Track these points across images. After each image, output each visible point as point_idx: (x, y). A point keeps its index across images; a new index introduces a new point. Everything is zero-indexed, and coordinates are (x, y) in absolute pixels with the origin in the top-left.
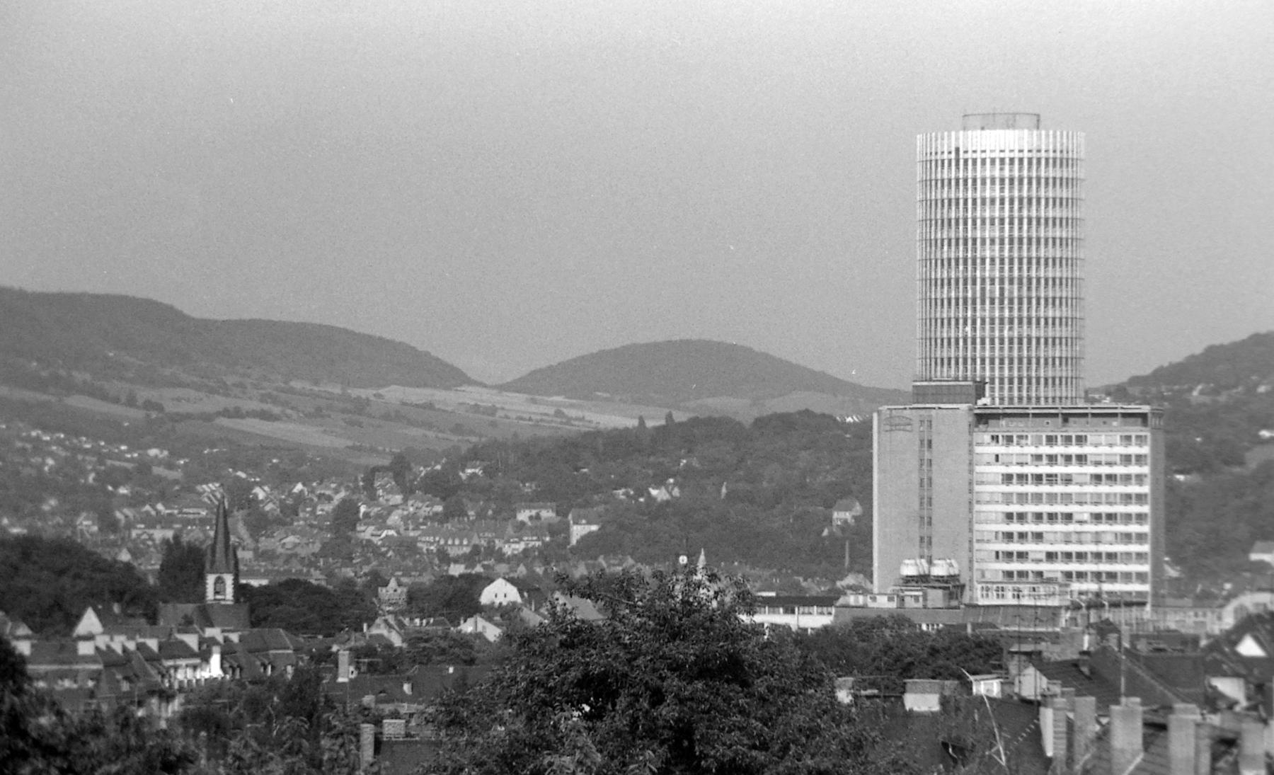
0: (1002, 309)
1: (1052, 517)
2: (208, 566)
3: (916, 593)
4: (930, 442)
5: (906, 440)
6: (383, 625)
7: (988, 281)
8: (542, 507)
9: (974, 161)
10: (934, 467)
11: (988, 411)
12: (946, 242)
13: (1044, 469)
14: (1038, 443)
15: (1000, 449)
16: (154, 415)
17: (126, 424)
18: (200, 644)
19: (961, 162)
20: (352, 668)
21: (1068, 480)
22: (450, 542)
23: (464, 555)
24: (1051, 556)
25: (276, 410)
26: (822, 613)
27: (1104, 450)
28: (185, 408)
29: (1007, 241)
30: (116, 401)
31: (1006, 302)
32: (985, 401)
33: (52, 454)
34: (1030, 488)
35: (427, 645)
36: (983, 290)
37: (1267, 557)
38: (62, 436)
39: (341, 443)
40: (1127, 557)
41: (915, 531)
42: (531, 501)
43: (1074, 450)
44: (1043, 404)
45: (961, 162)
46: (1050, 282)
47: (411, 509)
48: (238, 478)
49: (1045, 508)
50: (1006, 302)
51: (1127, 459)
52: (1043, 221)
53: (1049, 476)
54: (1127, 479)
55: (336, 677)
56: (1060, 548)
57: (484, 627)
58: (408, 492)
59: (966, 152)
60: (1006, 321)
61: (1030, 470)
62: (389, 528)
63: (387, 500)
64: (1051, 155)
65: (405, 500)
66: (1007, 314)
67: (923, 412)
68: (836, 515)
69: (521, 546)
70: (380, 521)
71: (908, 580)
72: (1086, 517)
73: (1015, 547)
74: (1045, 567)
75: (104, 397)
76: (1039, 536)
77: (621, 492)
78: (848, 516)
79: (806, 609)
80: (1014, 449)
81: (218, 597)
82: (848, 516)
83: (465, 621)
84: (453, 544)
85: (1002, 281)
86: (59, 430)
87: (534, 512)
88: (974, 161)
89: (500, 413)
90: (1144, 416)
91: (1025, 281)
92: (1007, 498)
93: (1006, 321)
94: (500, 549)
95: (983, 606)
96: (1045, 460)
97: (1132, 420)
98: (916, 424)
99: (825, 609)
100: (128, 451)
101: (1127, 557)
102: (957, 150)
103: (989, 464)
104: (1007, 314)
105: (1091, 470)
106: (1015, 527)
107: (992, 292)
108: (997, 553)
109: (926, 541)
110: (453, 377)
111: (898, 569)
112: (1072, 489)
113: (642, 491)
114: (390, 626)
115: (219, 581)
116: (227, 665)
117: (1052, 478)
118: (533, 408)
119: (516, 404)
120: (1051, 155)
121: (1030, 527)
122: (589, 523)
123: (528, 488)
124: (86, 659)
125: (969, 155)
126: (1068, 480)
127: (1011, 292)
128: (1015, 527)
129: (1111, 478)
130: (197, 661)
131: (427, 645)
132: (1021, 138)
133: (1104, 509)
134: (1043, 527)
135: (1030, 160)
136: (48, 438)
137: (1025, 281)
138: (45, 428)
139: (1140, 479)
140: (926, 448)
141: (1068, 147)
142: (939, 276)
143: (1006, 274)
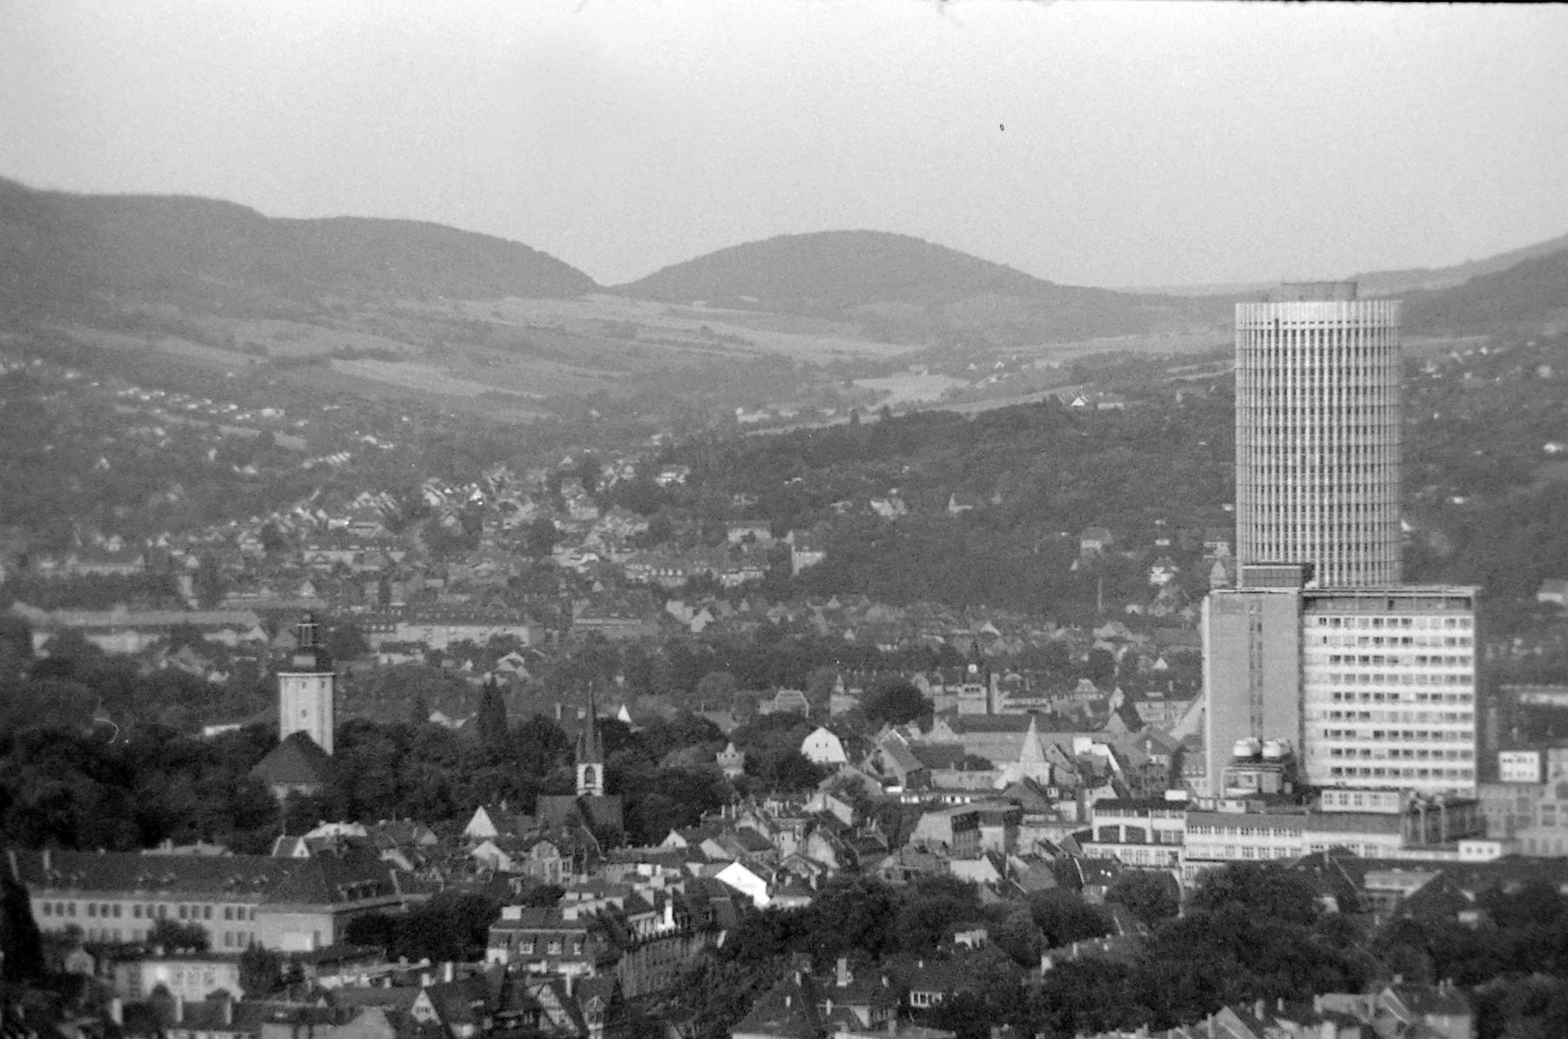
0: (1322, 477)
1: (1378, 696)
2: (578, 756)
3: (1250, 773)
4: (1260, 626)
5: (1238, 624)
6: (751, 818)
7: (1308, 451)
8: (756, 526)
9: (1294, 332)
10: (1264, 650)
11: (1317, 595)
12: (1266, 411)
13: (1371, 650)
14: (1364, 624)
15: (1327, 631)
16: (259, 360)
17: (230, 374)
18: (655, 897)
19: (1281, 333)
20: (849, 974)
21: (1394, 661)
22: (663, 573)
23: (679, 588)
24: (1378, 734)
25: (392, 346)
26: (1174, 817)
27: (1429, 633)
28: (292, 349)
29: (1326, 410)
30: (213, 343)
31: (1326, 470)
32: (1312, 585)
33: (161, 424)
34: (1358, 669)
35: (848, 891)
36: (1303, 458)
37: (1557, 598)
38: (163, 394)
39: (474, 389)
40: (1453, 736)
41: (1246, 711)
42: (747, 516)
43: (1400, 632)
44: (1370, 586)
45: (1281, 333)
46: (1369, 449)
47: (609, 526)
48: (367, 443)
49: (1372, 688)
50: (1326, 470)
51: (1451, 642)
52: (1361, 390)
53: (1405, 677)
54: (1451, 660)
55: (835, 982)
56: (1387, 727)
57: (833, 805)
58: (604, 503)
59: (1285, 323)
60: (1326, 489)
61: (1357, 651)
62: (589, 551)
63: (581, 514)
64: (1369, 325)
65: (602, 514)
66: (1326, 481)
67: (1253, 597)
68: (1085, 544)
69: (741, 577)
70: (577, 541)
71: (1241, 761)
72: (1412, 697)
73: (1343, 725)
74: (1372, 745)
75: (200, 338)
76: (1366, 715)
77: (839, 504)
78: (1097, 545)
79: (1160, 812)
80: (1342, 631)
81: (589, 785)
82: (1097, 545)
83: (811, 797)
84: (666, 575)
85: (1322, 449)
86: (159, 386)
87: (746, 532)
88: (1294, 332)
89: (640, 335)
90: (1467, 600)
91: (1344, 449)
92: (1335, 678)
93: (1326, 489)
94: (718, 580)
95: (1327, 813)
96: (1371, 642)
97: (1456, 603)
98: (1247, 606)
99: (1177, 813)
100: (241, 410)
101: (1453, 736)
102: (1277, 321)
103: (1317, 645)
104: (1326, 481)
105: (1415, 651)
106: (1344, 707)
107: (1312, 460)
108: (1326, 731)
109: (1257, 721)
110: (571, 282)
111: (1231, 752)
112: (1398, 670)
113: (862, 503)
114: (758, 820)
115: (589, 770)
116: (678, 916)
117: (1378, 659)
118: (677, 324)
119: (649, 312)
120: (1369, 325)
121: (1358, 707)
122: (812, 550)
123: (740, 500)
124: (570, 925)
125: (1289, 327)
126: (1394, 661)
127: (1331, 460)
128: (1344, 707)
129: (1436, 659)
130: (653, 914)
131: (848, 891)
132: (1339, 310)
133: (1431, 689)
134: (1371, 706)
135: (1349, 331)
136: (147, 398)
137: (1344, 449)
138: (147, 385)
139: (1464, 660)
140: (1255, 632)
141: (1365, 316)
142: (1259, 444)
143: (1326, 443)
